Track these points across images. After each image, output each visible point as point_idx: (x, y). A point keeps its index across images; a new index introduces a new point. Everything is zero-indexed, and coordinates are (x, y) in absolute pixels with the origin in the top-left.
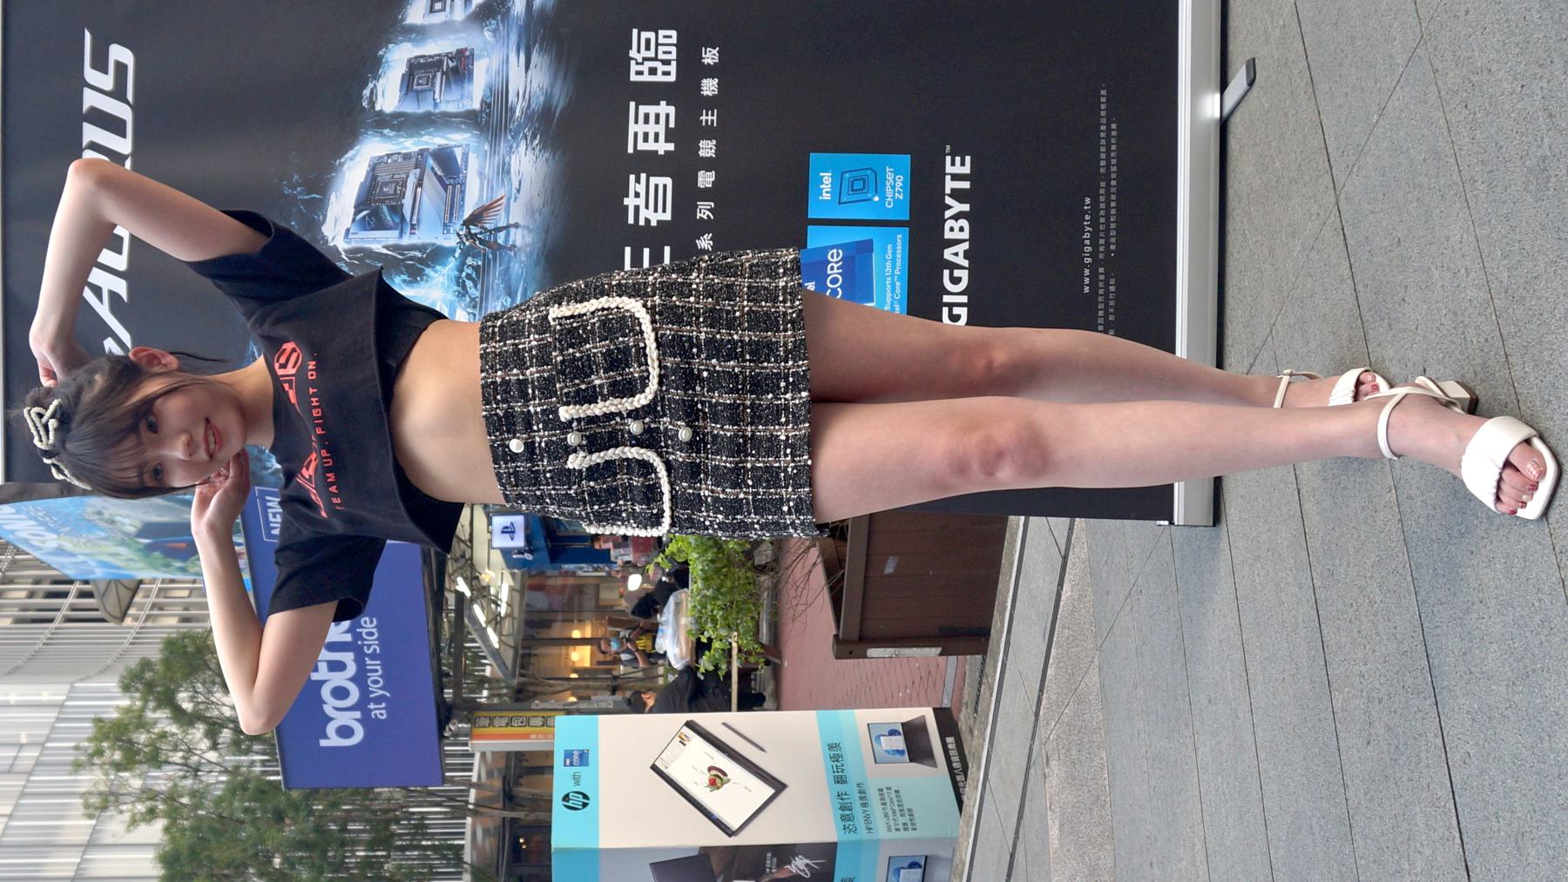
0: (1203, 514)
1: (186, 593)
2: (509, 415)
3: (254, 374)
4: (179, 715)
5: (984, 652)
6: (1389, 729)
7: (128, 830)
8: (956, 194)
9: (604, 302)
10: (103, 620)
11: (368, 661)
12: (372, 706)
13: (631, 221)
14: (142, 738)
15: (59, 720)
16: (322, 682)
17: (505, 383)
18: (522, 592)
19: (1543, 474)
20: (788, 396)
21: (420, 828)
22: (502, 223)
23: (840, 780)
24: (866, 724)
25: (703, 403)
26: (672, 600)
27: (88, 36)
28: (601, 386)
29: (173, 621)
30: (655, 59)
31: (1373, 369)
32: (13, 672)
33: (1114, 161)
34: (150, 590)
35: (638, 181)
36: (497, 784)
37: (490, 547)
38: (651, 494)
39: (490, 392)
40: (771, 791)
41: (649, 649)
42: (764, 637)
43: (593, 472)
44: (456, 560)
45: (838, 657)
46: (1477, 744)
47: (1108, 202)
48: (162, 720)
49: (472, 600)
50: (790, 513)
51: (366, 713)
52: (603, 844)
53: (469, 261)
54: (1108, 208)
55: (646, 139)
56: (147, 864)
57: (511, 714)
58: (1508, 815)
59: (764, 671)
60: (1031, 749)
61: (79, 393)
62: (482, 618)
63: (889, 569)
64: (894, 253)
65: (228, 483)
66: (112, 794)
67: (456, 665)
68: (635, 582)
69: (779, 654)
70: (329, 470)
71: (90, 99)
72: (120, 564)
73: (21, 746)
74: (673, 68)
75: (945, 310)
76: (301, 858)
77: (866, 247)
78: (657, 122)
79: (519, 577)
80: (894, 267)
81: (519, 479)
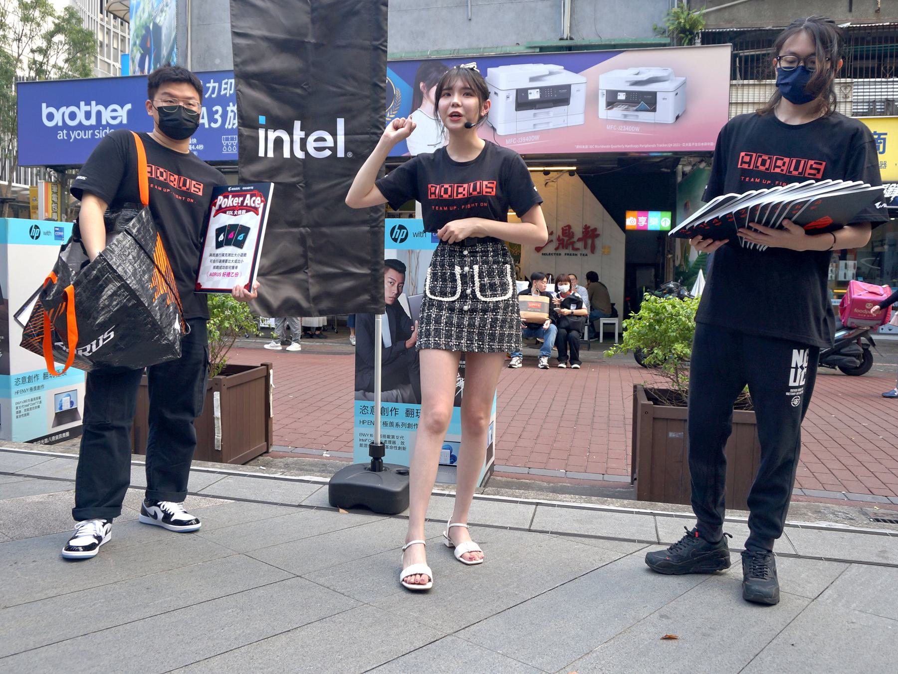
9: (511, 283)
11: (90, 132)
12: (65, 132)
16: (79, 108)
38: (443, 294)
43: (453, 275)
48: (49, 25)
51: (61, 129)
52: (9, 245)
57: (59, 203)
72: (138, 14)
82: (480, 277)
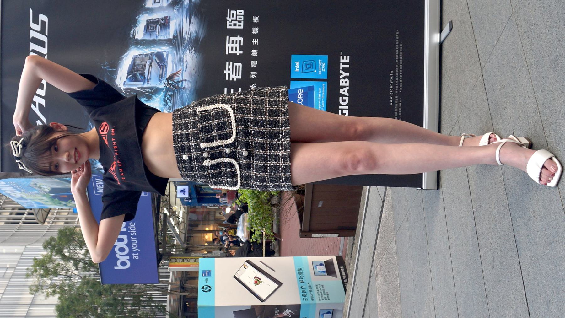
0: (433, 185)
1: (67, 213)
2: (183, 146)
3: (92, 133)
4: (64, 257)
5: (354, 235)
6: (501, 263)
7: (46, 299)
8: (344, 69)
9: (217, 105)
10: (37, 223)
12: (133, 254)
13: (227, 79)
14: (51, 266)
15: (21, 259)
16: (116, 245)
17: (181, 135)
18: (187, 214)
19: (556, 170)
20: (283, 140)
21: (150, 299)
22: (180, 80)
23: (302, 282)
24: (312, 261)
25: (252, 142)
26: (241, 216)
27: (31, 11)
28: (215, 136)
29: (62, 224)
30: (236, 20)
31: (495, 132)
32: (4, 242)
33: (401, 58)
34: (54, 212)
35: (229, 64)
36: (178, 283)
37: (176, 197)
39: (176, 138)
40: (277, 286)
41: (233, 235)
42: (275, 230)
43: (213, 167)
44: (164, 202)
45: (302, 237)
46: (533, 268)
47: (399, 72)
48: (58, 259)
49: (170, 217)
50: (283, 182)
51: (131, 257)
52: (216, 305)
53: (168, 93)
54: (399, 75)
55: (232, 49)
56: (52, 311)
57: (183, 258)
58: (544, 294)
59: (274, 243)
60: (371, 271)
61: (30, 137)
62: (173, 223)
63: (320, 206)
64: (322, 91)
65: (84, 173)
66: (40, 285)
67: (164, 240)
68: (228, 210)
69: (280, 237)
70: (120, 168)
71: (32, 34)
72: (44, 203)
73: (7, 268)
74: (242, 24)
75: (340, 111)
76: (108, 309)
77: (311, 89)
78: (236, 43)
79: (186, 208)
80: (321, 96)
81: (186, 168)
82: (212, 141)
